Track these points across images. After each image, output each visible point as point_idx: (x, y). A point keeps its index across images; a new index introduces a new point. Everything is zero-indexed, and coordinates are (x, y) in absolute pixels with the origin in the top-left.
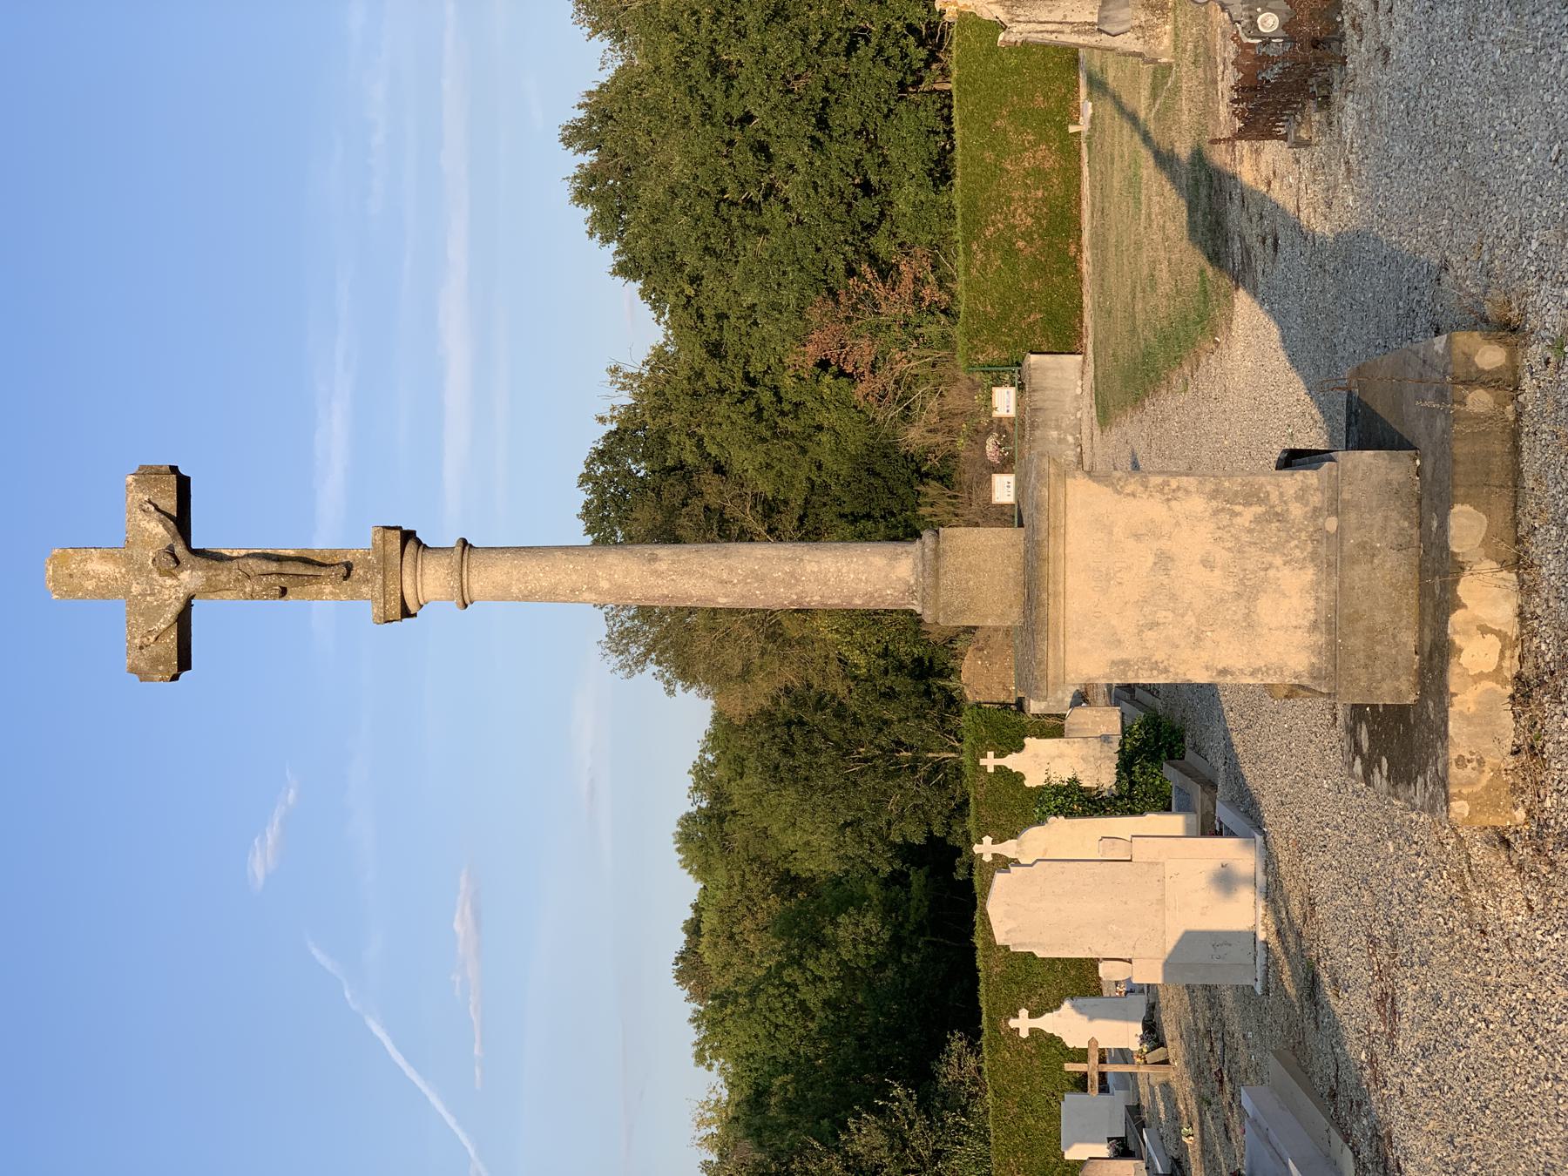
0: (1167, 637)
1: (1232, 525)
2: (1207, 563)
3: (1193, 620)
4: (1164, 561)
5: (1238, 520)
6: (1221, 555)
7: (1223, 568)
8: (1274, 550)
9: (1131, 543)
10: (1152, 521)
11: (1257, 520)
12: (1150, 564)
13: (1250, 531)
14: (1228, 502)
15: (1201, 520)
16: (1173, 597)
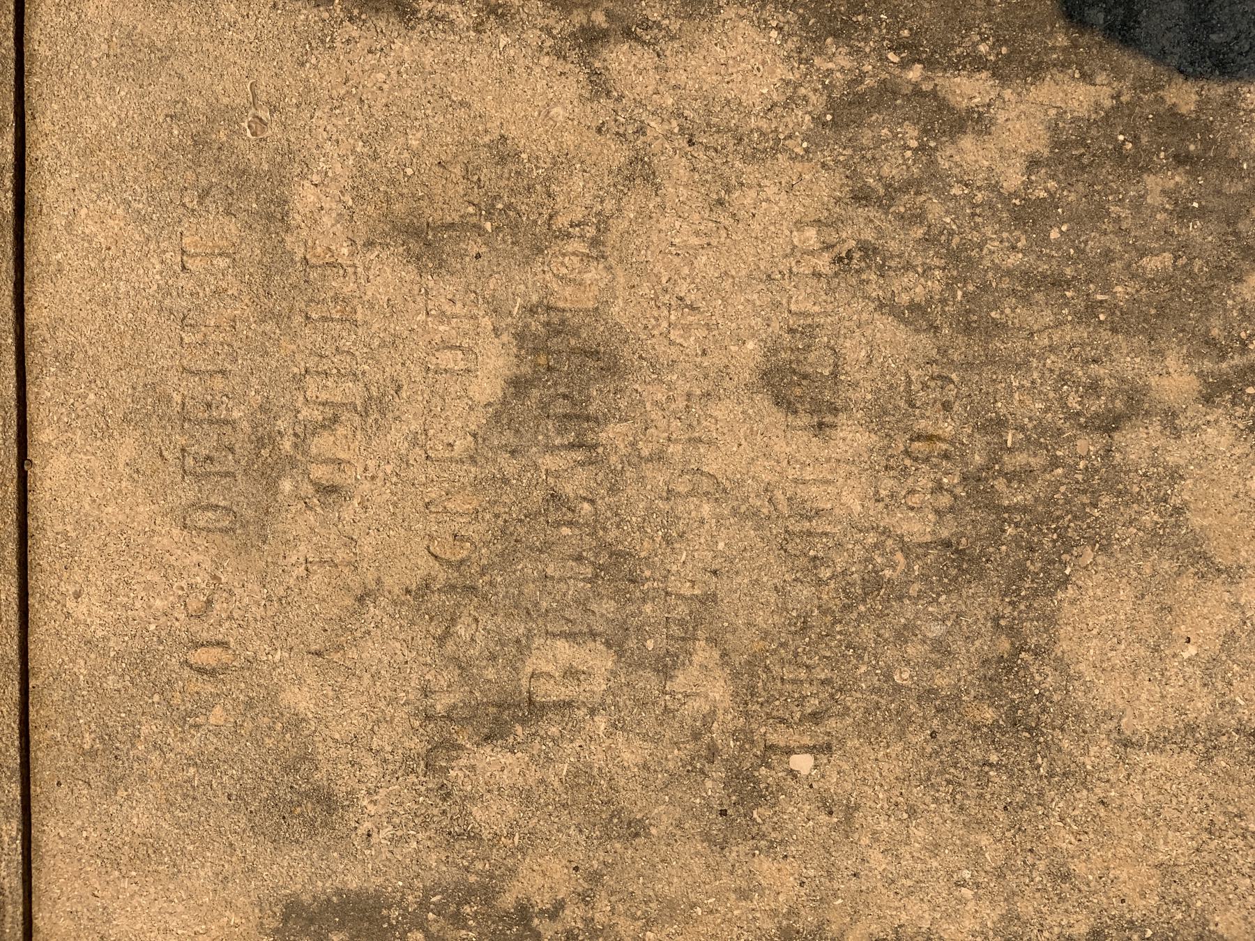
0: (581, 777)
1: (931, 179)
2: (795, 386)
3: (719, 691)
4: (566, 372)
5: (969, 152)
6: (872, 345)
7: (878, 416)
8: (1151, 320)
9: (386, 275)
10: (503, 152)
11: (1069, 150)
12: (487, 387)
13: (1027, 215)
14: (911, 51)
15: (765, 149)
16: (616, 568)
